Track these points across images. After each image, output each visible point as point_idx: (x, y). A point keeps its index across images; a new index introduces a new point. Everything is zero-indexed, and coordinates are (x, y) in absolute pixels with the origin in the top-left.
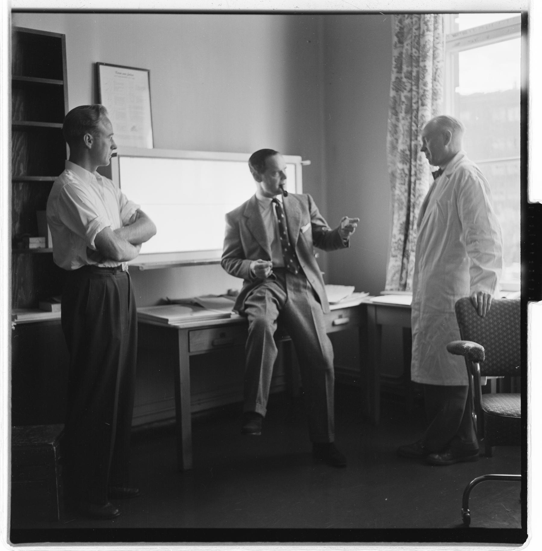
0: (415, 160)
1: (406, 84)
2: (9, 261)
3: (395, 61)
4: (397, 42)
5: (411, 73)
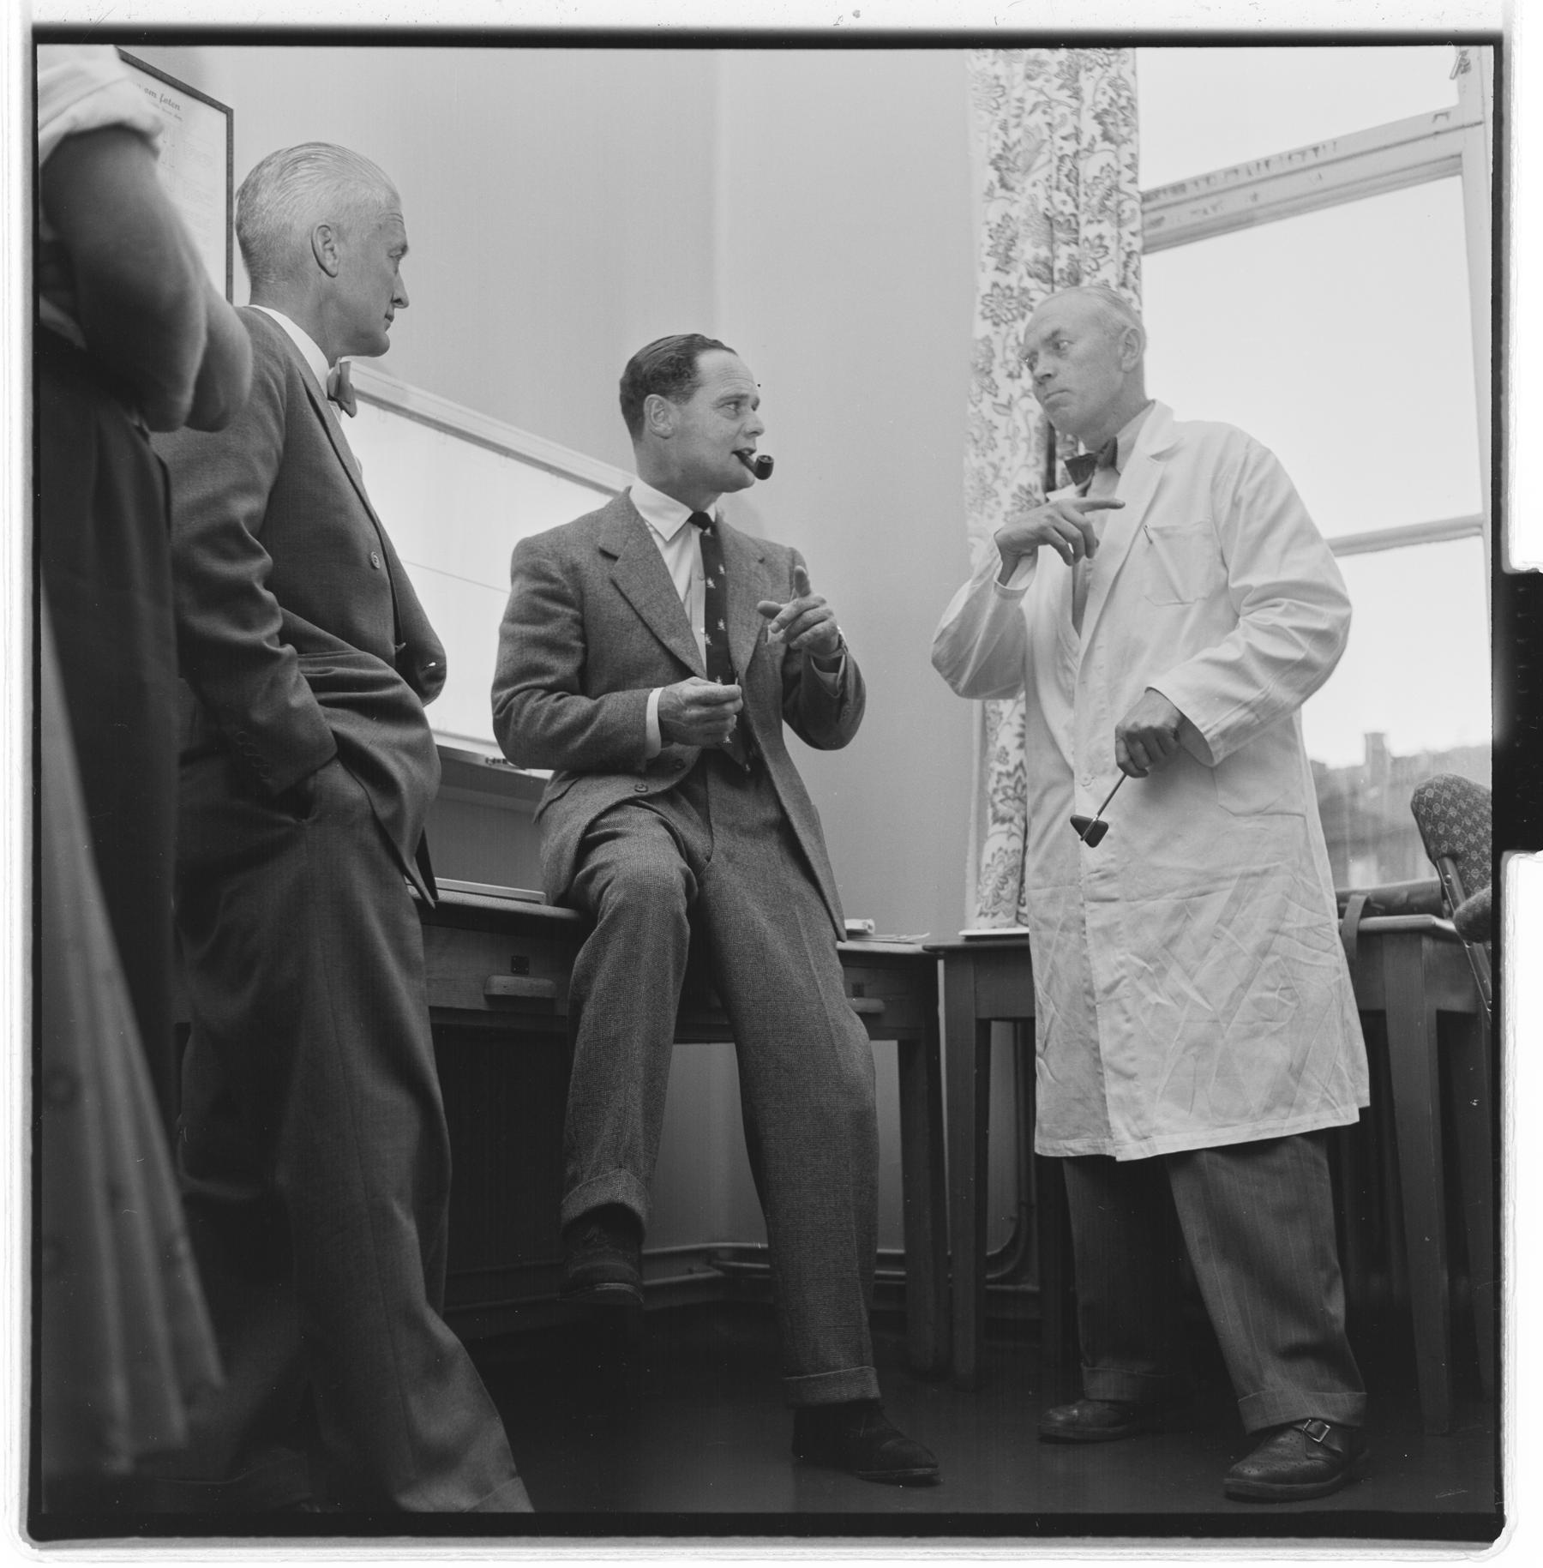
1: (1033, 294)
3: (991, 237)
4: (997, 185)
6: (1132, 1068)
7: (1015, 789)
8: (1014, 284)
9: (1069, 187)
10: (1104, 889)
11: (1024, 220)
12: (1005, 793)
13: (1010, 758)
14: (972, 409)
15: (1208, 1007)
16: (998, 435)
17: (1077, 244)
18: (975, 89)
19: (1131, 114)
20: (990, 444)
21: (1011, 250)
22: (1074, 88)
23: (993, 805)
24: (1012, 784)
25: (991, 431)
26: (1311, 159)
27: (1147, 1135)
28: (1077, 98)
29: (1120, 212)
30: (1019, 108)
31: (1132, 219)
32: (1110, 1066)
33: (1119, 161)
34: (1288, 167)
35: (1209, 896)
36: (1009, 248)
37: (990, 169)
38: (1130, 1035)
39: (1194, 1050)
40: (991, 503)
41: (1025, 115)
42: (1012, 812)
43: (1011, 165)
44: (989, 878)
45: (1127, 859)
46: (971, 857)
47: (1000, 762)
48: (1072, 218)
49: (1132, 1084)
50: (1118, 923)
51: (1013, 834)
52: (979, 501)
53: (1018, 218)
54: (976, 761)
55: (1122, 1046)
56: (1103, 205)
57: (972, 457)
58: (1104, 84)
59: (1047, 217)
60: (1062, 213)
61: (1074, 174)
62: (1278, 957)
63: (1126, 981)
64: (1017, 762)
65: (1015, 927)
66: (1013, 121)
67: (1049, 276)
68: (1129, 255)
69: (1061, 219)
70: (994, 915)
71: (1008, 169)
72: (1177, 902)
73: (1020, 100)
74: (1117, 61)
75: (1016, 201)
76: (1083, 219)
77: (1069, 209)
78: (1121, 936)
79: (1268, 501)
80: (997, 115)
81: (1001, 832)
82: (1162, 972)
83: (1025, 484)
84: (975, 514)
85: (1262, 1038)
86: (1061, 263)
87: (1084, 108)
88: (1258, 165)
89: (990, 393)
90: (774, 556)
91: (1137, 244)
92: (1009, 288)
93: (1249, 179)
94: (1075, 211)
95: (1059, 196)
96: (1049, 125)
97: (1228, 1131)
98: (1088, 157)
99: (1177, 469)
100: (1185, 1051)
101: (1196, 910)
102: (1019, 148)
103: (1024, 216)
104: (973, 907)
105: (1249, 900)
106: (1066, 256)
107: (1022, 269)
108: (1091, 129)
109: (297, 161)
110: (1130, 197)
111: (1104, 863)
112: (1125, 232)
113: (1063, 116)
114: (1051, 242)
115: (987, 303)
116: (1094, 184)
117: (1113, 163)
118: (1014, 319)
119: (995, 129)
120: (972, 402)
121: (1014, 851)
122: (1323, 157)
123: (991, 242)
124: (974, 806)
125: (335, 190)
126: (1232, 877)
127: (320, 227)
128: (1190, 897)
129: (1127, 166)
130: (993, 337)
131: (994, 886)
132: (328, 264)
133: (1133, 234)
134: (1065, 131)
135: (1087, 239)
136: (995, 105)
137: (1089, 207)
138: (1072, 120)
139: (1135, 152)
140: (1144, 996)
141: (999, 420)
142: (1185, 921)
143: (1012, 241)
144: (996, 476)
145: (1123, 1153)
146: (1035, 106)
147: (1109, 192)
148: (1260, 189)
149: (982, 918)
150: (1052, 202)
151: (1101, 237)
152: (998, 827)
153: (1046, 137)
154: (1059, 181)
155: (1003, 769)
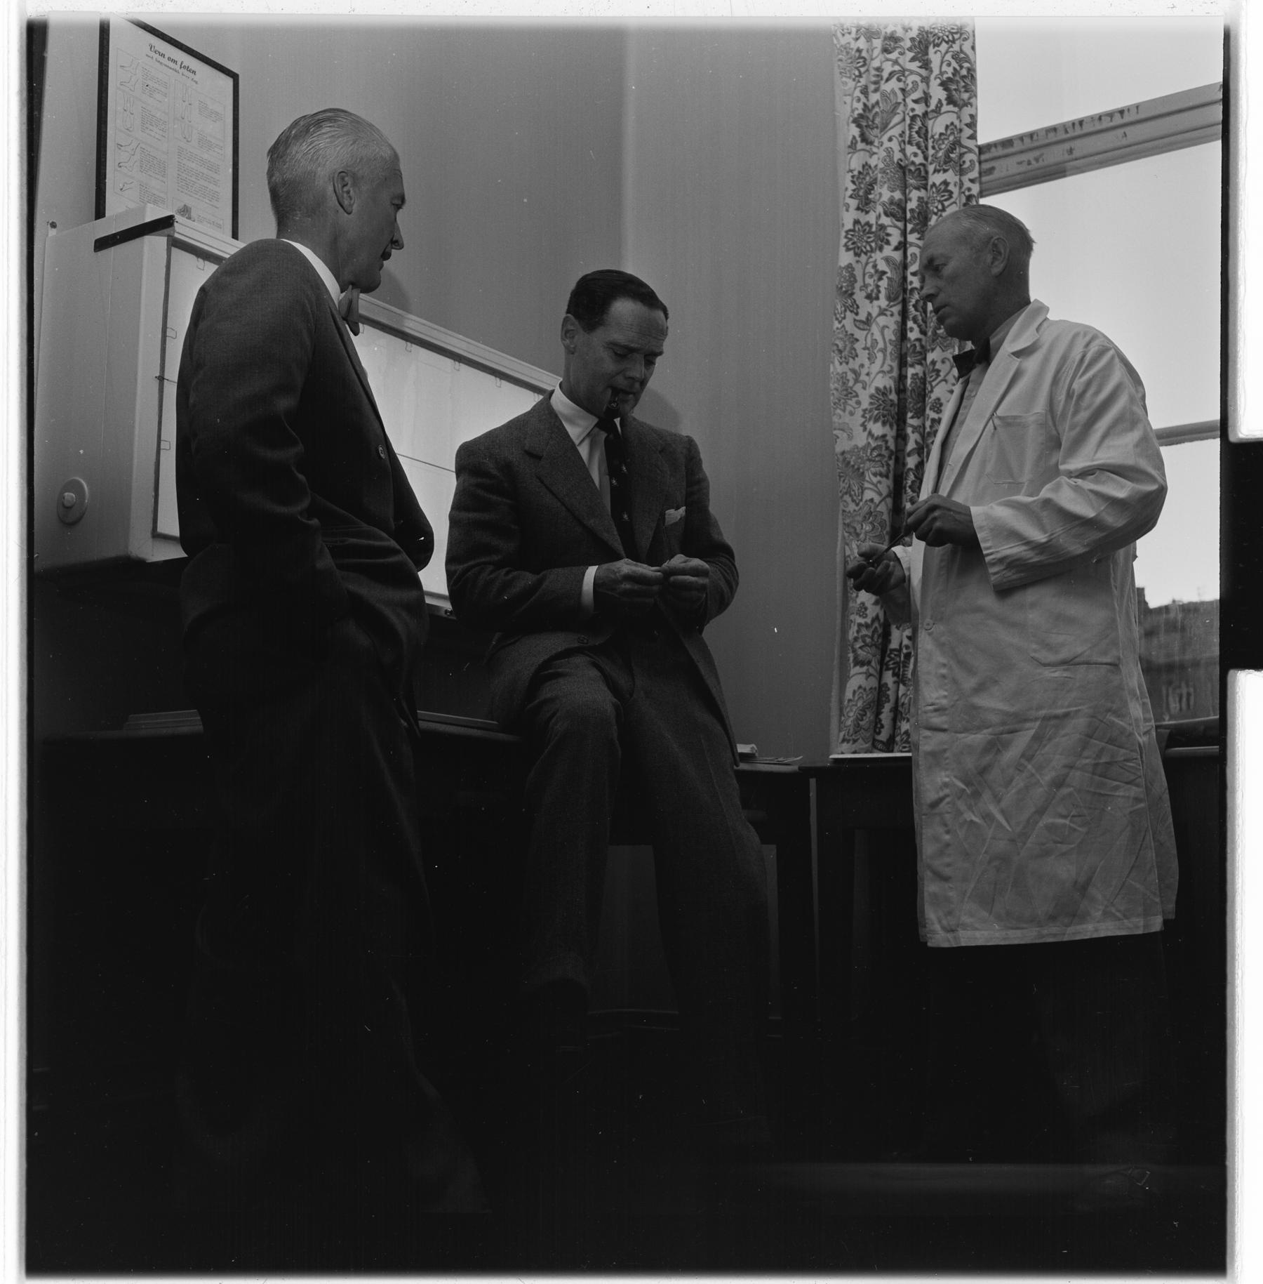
0: (920, 413)
1: (889, 230)
2: (20, 981)
3: (853, 182)
4: (859, 139)
5: (901, 206)
6: (947, 871)
7: (872, 638)
8: (873, 221)
9: (919, 142)
10: (937, 720)
11: (881, 169)
12: (864, 641)
13: (868, 612)
14: (836, 325)
15: (1008, 828)
16: (858, 346)
17: (926, 189)
18: (841, 60)
19: (971, 82)
20: (852, 354)
21: (870, 194)
22: (924, 61)
23: (854, 651)
24: (870, 634)
25: (852, 342)
26: (1118, 120)
27: (953, 928)
28: (926, 69)
29: (962, 163)
30: (878, 76)
31: (971, 169)
32: (929, 867)
33: (961, 121)
34: (1098, 127)
35: (1016, 734)
36: (868, 192)
37: (853, 126)
38: (948, 845)
39: (996, 863)
40: (852, 402)
41: (883, 82)
42: (870, 656)
43: (870, 123)
44: (851, 710)
45: (956, 698)
46: (834, 693)
47: (860, 616)
48: (922, 168)
49: (947, 885)
50: (945, 751)
51: (871, 675)
52: (842, 401)
53: (876, 166)
54: (839, 615)
55: (941, 853)
56: (947, 156)
57: (837, 363)
58: (948, 57)
59: (901, 167)
60: (913, 163)
61: (923, 131)
62: (1072, 789)
63: (948, 800)
64: (874, 615)
65: (871, 752)
66: (872, 87)
67: (903, 216)
68: (969, 198)
69: (913, 168)
70: (855, 741)
71: (867, 126)
72: (990, 737)
73: (879, 69)
74: (959, 38)
75: (875, 153)
76: (931, 168)
77: (919, 160)
78: (947, 761)
79: (1097, 393)
80: (859, 82)
81: (860, 673)
82: (977, 795)
83: (881, 386)
84: (838, 411)
85: (1053, 857)
86: (912, 205)
87: (932, 77)
88: (1074, 124)
89: (851, 311)
90: (674, 446)
91: (975, 189)
92: (868, 224)
93: (1065, 136)
94: (924, 162)
95: (910, 150)
96: (903, 90)
97: (1019, 933)
98: (937, 117)
99: (1032, 364)
100: (990, 862)
101: (1006, 745)
102: (877, 109)
103: (881, 165)
104: (836, 734)
105: (1050, 739)
106: (917, 199)
107: (880, 209)
108: (938, 94)
109: (324, 120)
110: (970, 151)
111: (937, 698)
112: (965, 179)
113: (914, 83)
114: (904, 188)
115: (850, 236)
116: (940, 139)
117: (957, 122)
118: (872, 251)
119: (857, 93)
120: (837, 319)
121: (871, 688)
122: (1128, 118)
123: (854, 187)
124: (836, 652)
125: (351, 145)
126: (1036, 719)
127: (340, 173)
128: (1002, 733)
129: (967, 125)
130: (854, 265)
131: (855, 717)
132: (346, 203)
133: (972, 181)
134: (916, 96)
135: (934, 184)
136: (857, 73)
137: (936, 158)
138: (922, 86)
139: (974, 114)
140: (962, 814)
141: (859, 334)
142: (996, 754)
143: (871, 187)
144: (856, 381)
145: (933, 941)
146: (891, 75)
147: (952, 146)
148: (1077, 144)
149: (845, 744)
150: (905, 155)
151: (946, 183)
152: (858, 669)
153: (900, 100)
154: (910, 136)
155: (862, 621)
